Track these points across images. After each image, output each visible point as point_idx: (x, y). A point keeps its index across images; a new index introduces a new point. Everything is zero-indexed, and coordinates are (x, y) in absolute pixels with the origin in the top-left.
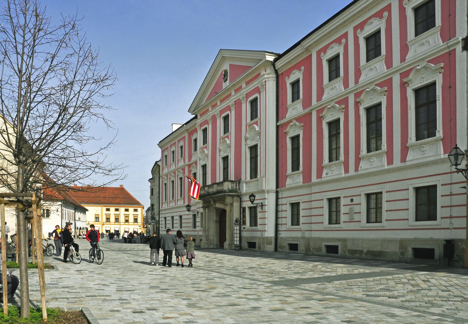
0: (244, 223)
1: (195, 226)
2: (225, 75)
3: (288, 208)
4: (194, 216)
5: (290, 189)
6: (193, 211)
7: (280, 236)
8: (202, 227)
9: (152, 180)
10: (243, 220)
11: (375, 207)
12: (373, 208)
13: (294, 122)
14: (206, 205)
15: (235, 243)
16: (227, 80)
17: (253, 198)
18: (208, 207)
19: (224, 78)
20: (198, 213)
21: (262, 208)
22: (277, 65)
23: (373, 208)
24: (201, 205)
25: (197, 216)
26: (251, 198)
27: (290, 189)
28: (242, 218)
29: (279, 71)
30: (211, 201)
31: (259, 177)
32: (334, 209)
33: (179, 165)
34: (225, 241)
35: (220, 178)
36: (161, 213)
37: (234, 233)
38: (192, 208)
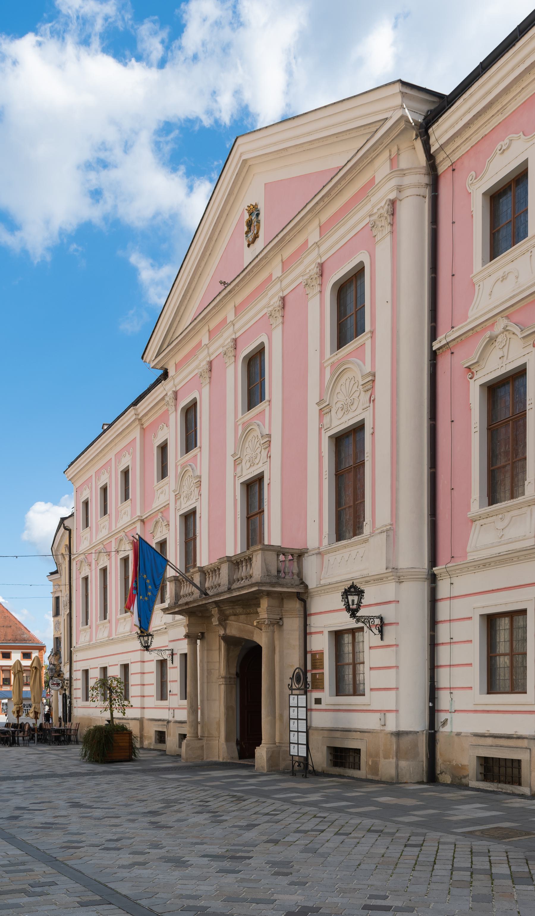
0: (318, 685)
1: (163, 695)
2: (249, 224)
3: (473, 631)
4: (162, 664)
5: (485, 564)
6: (159, 650)
7: (444, 731)
8: (184, 696)
9: (56, 576)
10: (314, 676)
11: (508, 651)
12: (504, 655)
13: (501, 323)
14: (198, 630)
15: (294, 751)
16: (256, 237)
17: (356, 598)
18: (202, 637)
19: (247, 233)
20: (172, 655)
21: (381, 632)
22: (438, 133)
23: (504, 655)
24: (182, 631)
25: (169, 663)
26: (350, 598)
27: (485, 564)
28: (309, 667)
29: (439, 158)
30: (212, 616)
31: (367, 529)
32: (503, 647)
33: (119, 525)
34: (259, 743)
35: (233, 546)
36: (74, 658)
37: (297, 721)
38: (156, 642)
